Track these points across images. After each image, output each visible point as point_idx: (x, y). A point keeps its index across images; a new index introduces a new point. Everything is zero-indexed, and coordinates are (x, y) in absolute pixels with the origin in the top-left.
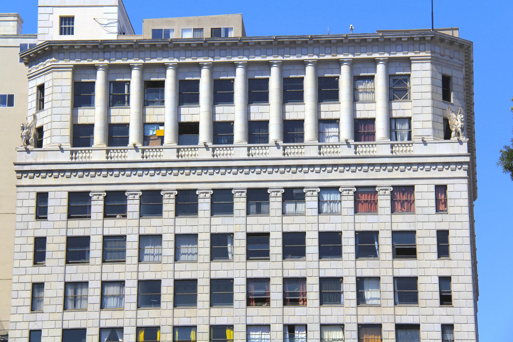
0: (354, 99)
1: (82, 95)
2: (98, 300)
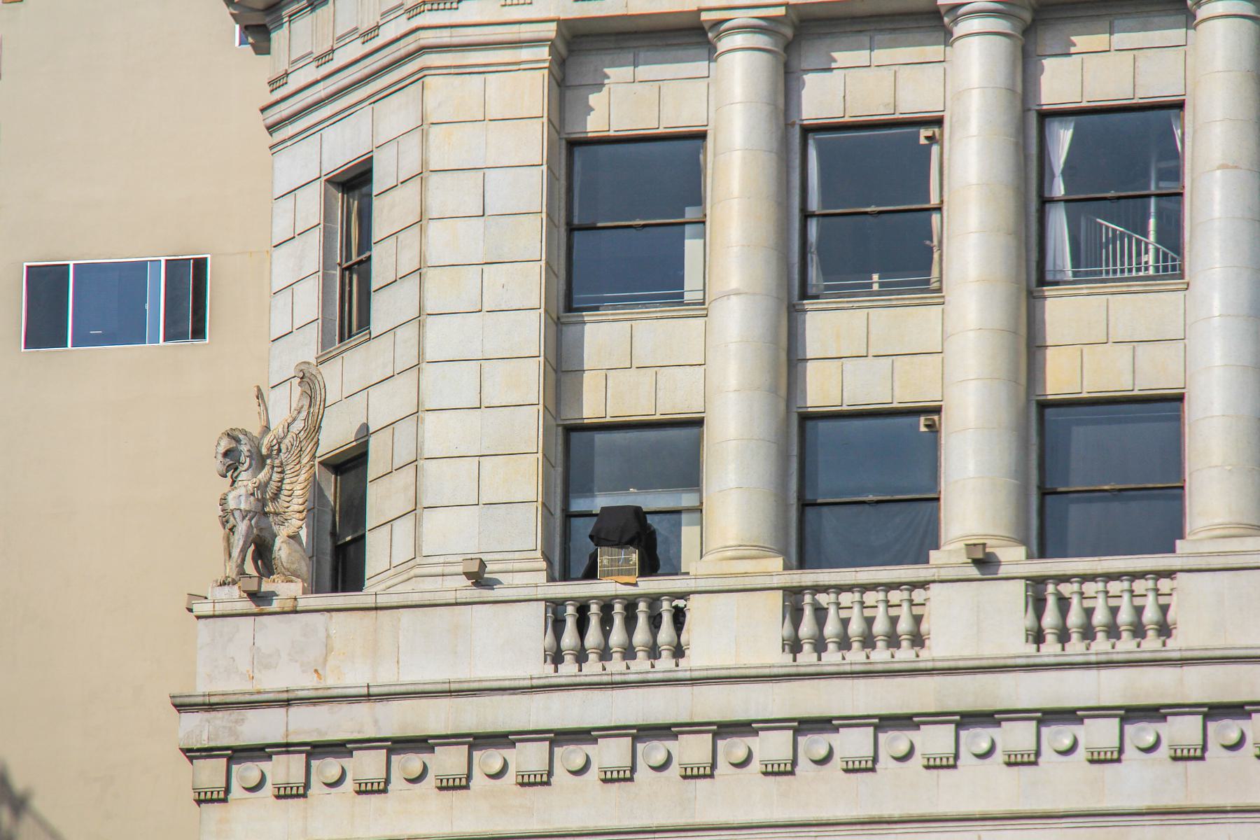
1: (615, 224)
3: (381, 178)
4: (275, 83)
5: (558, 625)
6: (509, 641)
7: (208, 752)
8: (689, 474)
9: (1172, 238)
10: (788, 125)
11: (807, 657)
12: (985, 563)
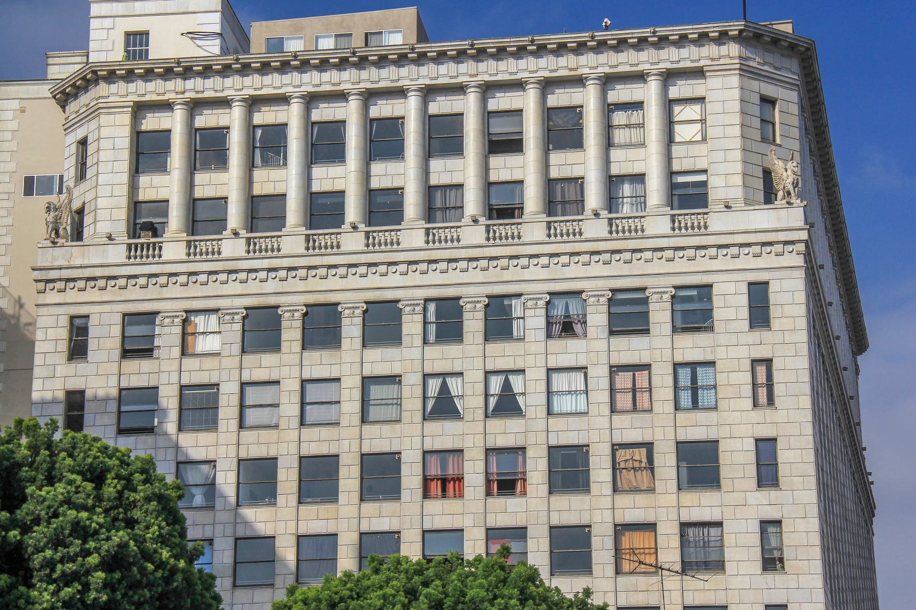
0: (608, 143)
1: (147, 151)
2: (356, 407)
3: (90, 141)
4: (66, 119)
5: (130, 251)
6: (117, 253)
7: (40, 281)
8: (166, 215)
9: (285, 158)
10: (191, 128)
11: (311, 251)
12: (236, 234)
